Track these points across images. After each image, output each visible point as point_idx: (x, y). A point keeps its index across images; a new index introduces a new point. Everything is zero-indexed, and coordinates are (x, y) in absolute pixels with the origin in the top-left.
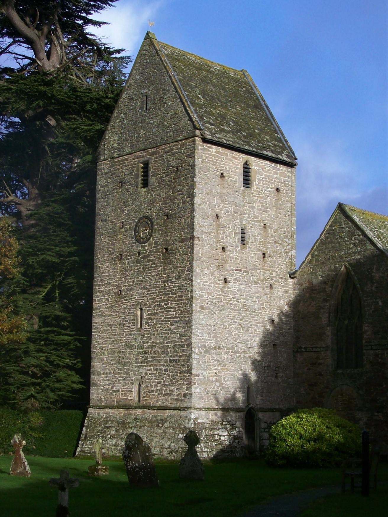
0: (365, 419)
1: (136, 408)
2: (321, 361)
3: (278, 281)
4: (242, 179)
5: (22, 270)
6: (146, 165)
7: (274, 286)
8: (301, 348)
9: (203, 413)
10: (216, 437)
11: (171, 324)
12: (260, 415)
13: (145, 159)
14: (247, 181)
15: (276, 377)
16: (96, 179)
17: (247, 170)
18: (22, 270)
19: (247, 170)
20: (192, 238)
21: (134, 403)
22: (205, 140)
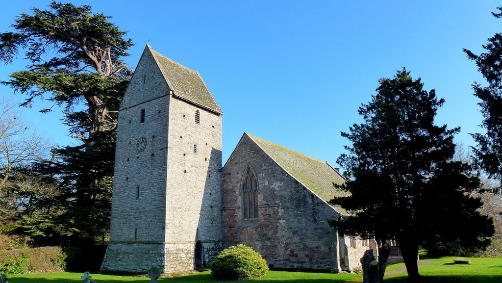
0: (260, 245)
1: (134, 243)
2: (236, 215)
3: (213, 173)
4: (194, 119)
5: (459, 250)
6: (143, 111)
7: (211, 176)
8: (225, 208)
9: (172, 245)
10: (179, 259)
11: (155, 195)
12: (204, 245)
13: (143, 108)
14: (197, 120)
15: (212, 223)
16: (184, 277)
17: (197, 113)
18: (459, 250)
19: (197, 113)
20: (167, 148)
21: (133, 240)
22: (174, 96)
